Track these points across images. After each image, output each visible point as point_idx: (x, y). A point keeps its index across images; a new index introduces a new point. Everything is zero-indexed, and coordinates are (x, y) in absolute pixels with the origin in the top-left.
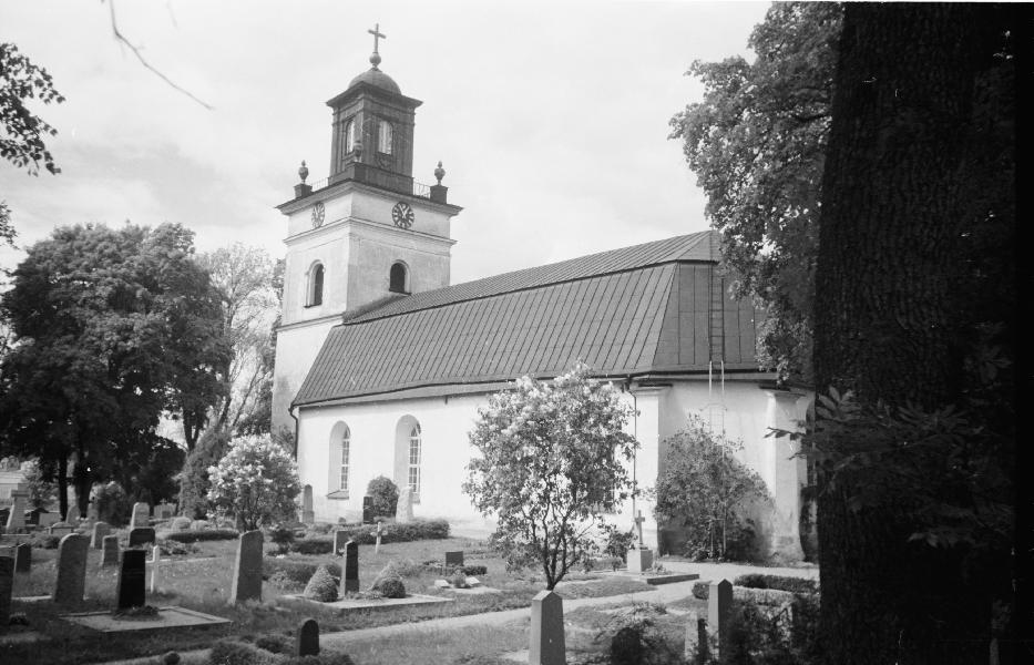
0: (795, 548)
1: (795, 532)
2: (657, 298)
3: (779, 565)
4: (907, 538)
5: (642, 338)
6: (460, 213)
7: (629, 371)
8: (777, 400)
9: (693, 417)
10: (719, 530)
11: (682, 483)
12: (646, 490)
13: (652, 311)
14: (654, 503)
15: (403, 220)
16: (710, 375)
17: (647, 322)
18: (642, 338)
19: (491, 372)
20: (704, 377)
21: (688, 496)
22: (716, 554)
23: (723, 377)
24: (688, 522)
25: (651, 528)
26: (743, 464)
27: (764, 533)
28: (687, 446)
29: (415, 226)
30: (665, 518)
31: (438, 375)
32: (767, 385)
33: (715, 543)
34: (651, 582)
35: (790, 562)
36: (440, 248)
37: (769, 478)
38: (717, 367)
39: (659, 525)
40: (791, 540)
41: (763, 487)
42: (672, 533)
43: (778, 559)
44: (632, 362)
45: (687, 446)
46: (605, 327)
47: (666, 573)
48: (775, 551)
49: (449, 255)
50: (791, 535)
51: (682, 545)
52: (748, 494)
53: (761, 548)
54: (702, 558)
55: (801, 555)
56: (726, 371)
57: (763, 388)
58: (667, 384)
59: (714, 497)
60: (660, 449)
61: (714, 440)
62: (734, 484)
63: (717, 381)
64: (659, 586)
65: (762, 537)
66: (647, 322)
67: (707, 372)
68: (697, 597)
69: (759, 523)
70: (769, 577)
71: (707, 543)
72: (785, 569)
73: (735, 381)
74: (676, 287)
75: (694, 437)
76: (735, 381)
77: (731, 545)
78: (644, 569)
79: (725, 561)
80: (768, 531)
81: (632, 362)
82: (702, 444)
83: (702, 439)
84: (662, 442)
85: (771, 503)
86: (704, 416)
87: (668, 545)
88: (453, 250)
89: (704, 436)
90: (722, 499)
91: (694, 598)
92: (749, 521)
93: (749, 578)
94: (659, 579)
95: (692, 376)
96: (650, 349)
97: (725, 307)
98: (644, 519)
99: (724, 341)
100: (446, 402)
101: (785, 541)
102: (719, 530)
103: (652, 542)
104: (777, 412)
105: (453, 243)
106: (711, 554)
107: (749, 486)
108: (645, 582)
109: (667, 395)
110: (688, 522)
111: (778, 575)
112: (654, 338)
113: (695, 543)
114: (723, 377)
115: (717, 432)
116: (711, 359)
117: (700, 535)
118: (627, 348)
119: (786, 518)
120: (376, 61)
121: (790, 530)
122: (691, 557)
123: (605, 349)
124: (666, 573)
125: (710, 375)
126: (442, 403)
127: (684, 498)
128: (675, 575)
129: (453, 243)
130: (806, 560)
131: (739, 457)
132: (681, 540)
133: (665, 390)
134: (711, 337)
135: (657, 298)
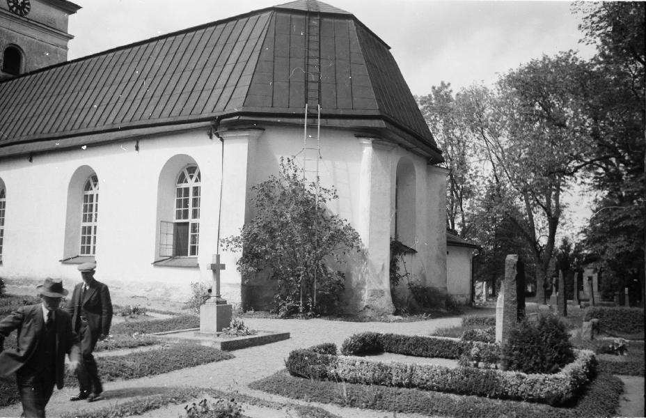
0: (385, 302)
1: (386, 285)
2: (251, 43)
3: (371, 320)
4: (24, 365)
5: (233, 81)
6: (78, 11)
7: (217, 114)
8: (373, 147)
9: (285, 162)
10: (309, 283)
11: (271, 232)
12: (230, 240)
13: (245, 56)
14: (239, 254)
15: (18, 7)
16: (306, 119)
17: (240, 67)
18: (233, 81)
19: (76, 127)
20: (300, 121)
21: (278, 246)
22: (306, 309)
23: (319, 122)
24: (276, 275)
25: (234, 282)
26: (335, 213)
27: (354, 285)
28: (277, 193)
29: (31, 15)
30: (251, 269)
31: (25, 133)
32: (361, 133)
33: (305, 298)
34: (228, 347)
35: (381, 316)
36: (56, 40)
37: (362, 228)
38: (313, 111)
39: (244, 278)
40: (382, 292)
41: (356, 238)
42: (258, 287)
43: (369, 313)
44: (221, 105)
45: (277, 193)
46: (196, 74)
47: (73, 311)
48: (365, 304)
49: (66, 48)
50: (381, 288)
51: (269, 300)
52: (339, 245)
53: (351, 301)
54: (291, 313)
55: (391, 308)
56: (323, 116)
57: (358, 136)
58: (261, 127)
59: (308, 247)
60: (248, 195)
61: (307, 187)
62: (328, 234)
63: (312, 128)
64: (236, 353)
65: (351, 290)
66: (240, 67)
67: (302, 116)
68: (294, 374)
69: (350, 274)
70: (388, 337)
71: (296, 298)
72: (378, 324)
73: (331, 128)
74: (272, 34)
75: (286, 184)
76: (331, 128)
77: (322, 300)
78: (219, 329)
79: (314, 316)
80: (358, 284)
81: (221, 105)
82: (294, 191)
83: (294, 187)
84: (251, 188)
85: (363, 255)
86: (299, 162)
87: (253, 300)
88: (70, 43)
89: (296, 184)
90: (315, 248)
91: (288, 374)
92: (339, 273)
93: (363, 339)
94: (237, 342)
95: (287, 121)
96: (242, 91)
97: (323, 55)
98: (223, 267)
99: (320, 87)
100: (31, 161)
101: (377, 293)
102: (309, 283)
103: (233, 296)
104: (373, 161)
105: (71, 37)
106: (301, 309)
107: (343, 237)
108: (219, 347)
109: (258, 139)
110: (276, 275)
111: (399, 333)
112: (246, 80)
113: (284, 298)
114: (319, 122)
115: (311, 178)
116: (306, 102)
117: (289, 288)
118: (217, 92)
119: (378, 271)
120: (218, 257)
121: (381, 283)
122: (278, 312)
123: (195, 95)
124: (73, 311)
125: (306, 119)
126: (27, 162)
127: (273, 247)
128: (260, 335)
129: (71, 37)
130: (395, 314)
131: (331, 207)
132: (267, 295)
133: (255, 133)
134: (307, 82)
135: (251, 43)
